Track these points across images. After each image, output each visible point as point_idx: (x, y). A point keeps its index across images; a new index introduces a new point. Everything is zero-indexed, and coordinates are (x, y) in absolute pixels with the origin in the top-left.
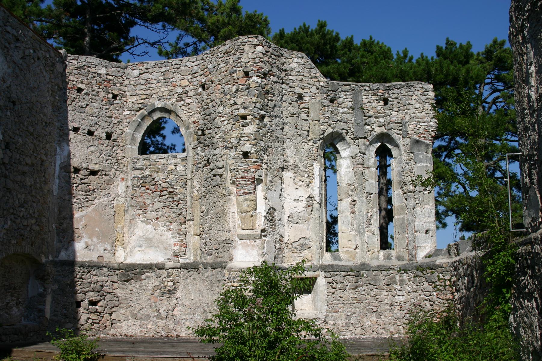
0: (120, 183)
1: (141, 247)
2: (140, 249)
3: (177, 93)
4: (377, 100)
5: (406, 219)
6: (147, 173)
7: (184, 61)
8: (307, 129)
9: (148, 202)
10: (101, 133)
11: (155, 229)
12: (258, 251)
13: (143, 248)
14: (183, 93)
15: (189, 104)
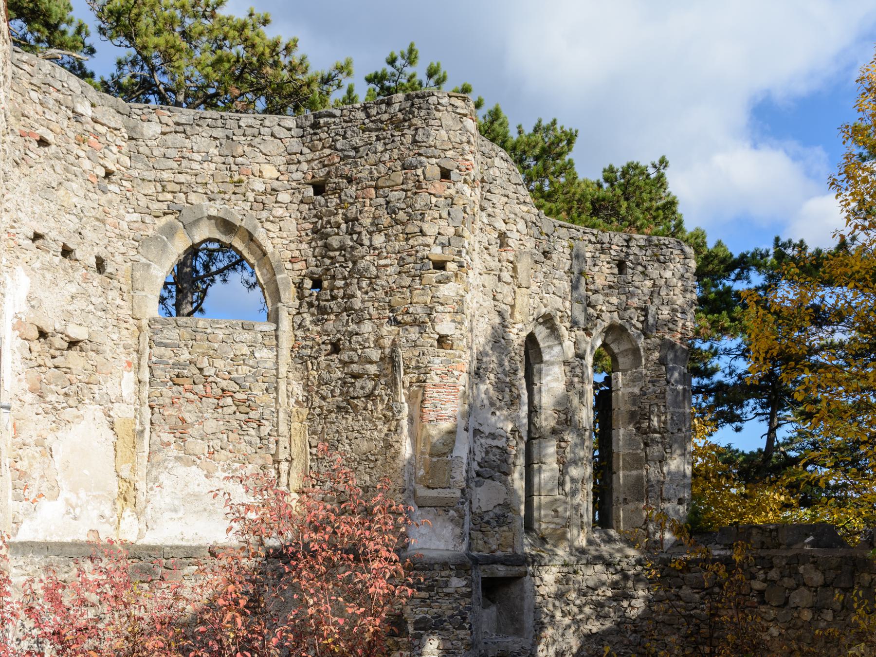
0: (125, 373)
1: (175, 511)
2: (173, 515)
3: (253, 190)
4: (608, 263)
5: (645, 479)
6: (185, 356)
7: (267, 123)
8: (509, 300)
9: (190, 418)
10: (86, 255)
11: (206, 476)
12: (453, 529)
13: (180, 514)
14: (265, 193)
15: (281, 219)
